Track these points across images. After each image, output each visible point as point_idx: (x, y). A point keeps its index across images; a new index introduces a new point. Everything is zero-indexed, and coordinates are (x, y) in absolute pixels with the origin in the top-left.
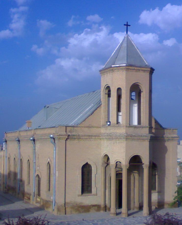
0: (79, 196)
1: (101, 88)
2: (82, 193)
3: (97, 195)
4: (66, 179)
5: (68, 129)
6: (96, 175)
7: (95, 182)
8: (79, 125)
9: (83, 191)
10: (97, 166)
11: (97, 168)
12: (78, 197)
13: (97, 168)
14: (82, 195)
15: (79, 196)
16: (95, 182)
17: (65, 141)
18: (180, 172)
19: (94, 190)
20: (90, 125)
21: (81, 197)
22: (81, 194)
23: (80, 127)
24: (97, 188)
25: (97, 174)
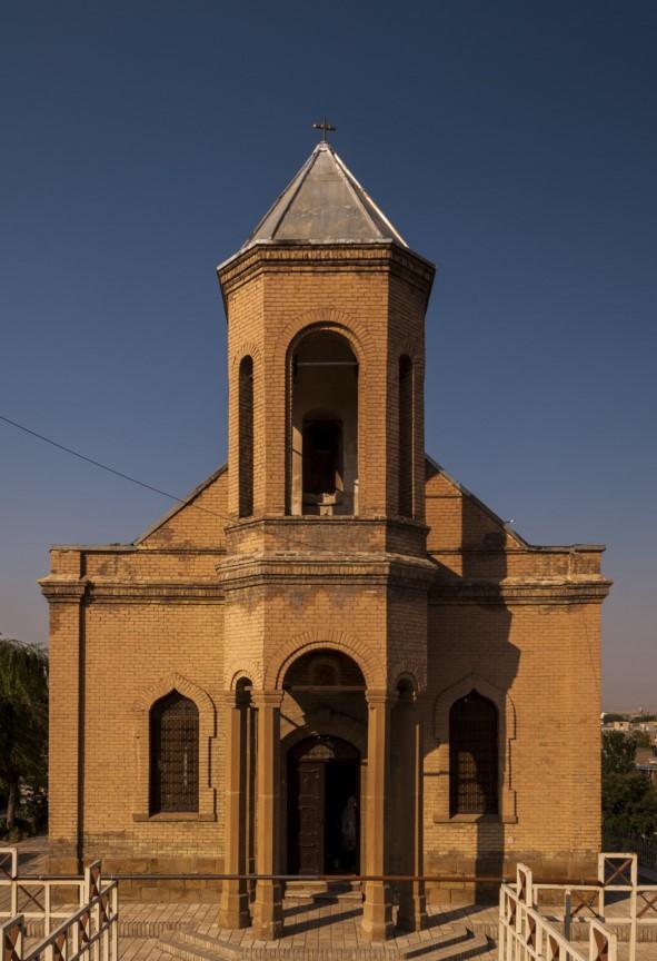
0: (138, 819)
1: (33, 841)
2: (451, 808)
3: (216, 821)
4: (87, 717)
5: (94, 562)
6: (215, 733)
7: (210, 770)
8: (141, 543)
9: (156, 806)
10: (214, 707)
11: (216, 712)
12: (476, 934)
13: (216, 712)
14: (153, 818)
15: (138, 819)
16: (210, 770)
17: (77, 607)
18: (233, 789)
19: (205, 799)
20: (187, 542)
21: (149, 825)
22: (147, 812)
23: (142, 552)
24: (215, 791)
25: (218, 735)
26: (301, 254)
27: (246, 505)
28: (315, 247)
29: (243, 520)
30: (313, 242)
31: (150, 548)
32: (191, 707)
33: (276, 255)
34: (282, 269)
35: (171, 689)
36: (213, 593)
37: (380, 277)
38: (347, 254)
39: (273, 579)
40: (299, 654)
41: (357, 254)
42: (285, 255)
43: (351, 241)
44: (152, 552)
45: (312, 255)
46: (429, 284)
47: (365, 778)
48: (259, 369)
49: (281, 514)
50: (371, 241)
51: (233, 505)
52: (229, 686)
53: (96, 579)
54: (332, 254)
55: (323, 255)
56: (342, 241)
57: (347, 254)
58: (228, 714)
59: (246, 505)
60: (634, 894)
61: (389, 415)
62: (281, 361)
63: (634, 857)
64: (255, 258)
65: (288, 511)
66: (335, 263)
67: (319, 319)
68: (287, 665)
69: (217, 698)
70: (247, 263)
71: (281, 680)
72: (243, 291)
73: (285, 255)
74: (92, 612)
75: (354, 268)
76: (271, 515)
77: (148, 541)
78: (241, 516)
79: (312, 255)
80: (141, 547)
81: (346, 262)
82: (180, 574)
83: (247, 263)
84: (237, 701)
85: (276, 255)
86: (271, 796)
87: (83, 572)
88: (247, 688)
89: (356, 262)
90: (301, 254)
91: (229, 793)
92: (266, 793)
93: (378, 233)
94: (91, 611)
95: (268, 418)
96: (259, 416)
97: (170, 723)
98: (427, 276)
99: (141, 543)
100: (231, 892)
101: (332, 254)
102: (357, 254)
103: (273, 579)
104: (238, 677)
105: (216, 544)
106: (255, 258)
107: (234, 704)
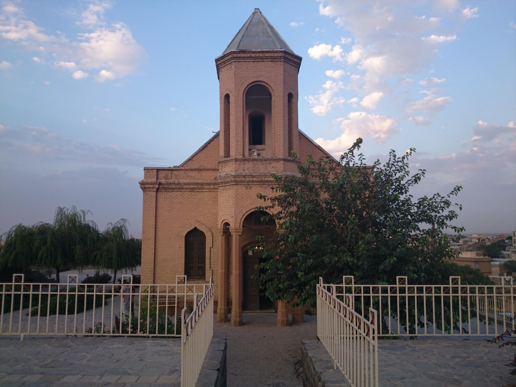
5: (162, 174)
18: (222, 269)
23: (183, 170)
26: (248, 55)
27: (227, 154)
28: (254, 52)
29: (226, 159)
30: (253, 50)
31: (186, 168)
32: (202, 235)
33: (239, 55)
34: (256, 60)
35: (193, 227)
36: (215, 186)
37: (280, 63)
38: (267, 55)
39: (238, 181)
40: (249, 213)
41: (271, 55)
42: (243, 55)
43: (268, 50)
44: (187, 170)
45: (253, 55)
46: (299, 65)
47: (239, 261)
48: (232, 99)
49: (241, 157)
50: (276, 50)
51: (222, 153)
52: (220, 226)
53: (163, 181)
54: (261, 55)
55: (258, 55)
56: (265, 50)
57: (267, 55)
58: (220, 240)
59: (227, 154)
60: (113, 296)
61: (284, 117)
62: (241, 96)
63: (14, 275)
64: (231, 56)
65: (244, 155)
66: (262, 58)
67: (256, 80)
68: (244, 217)
69: (213, 231)
70: (227, 58)
71: (242, 223)
72: (225, 68)
73: (243, 55)
74: (162, 195)
75: (270, 60)
76: (237, 157)
77: (185, 165)
78: (225, 157)
79: (253, 55)
80: (182, 168)
81: (267, 58)
82: (198, 179)
83: (227, 58)
84: (223, 232)
85: (239, 55)
86: (224, 271)
87: (157, 179)
88: (228, 227)
89: (271, 58)
90: (248, 55)
91: (220, 271)
92: (236, 270)
93: (279, 46)
94: (159, 193)
95: (236, 119)
96: (232, 118)
97: (194, 240)
98: (299, 62)
99: (182, 166)
100: (236, 317)
101: (261, 55)
102: (271, 55)
103: (238, 181)
104: (224, 222)
105: (213, 167)
106: (231, 56)
107: (222, 234)
